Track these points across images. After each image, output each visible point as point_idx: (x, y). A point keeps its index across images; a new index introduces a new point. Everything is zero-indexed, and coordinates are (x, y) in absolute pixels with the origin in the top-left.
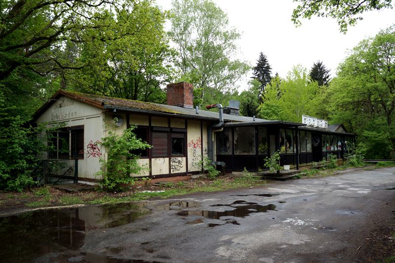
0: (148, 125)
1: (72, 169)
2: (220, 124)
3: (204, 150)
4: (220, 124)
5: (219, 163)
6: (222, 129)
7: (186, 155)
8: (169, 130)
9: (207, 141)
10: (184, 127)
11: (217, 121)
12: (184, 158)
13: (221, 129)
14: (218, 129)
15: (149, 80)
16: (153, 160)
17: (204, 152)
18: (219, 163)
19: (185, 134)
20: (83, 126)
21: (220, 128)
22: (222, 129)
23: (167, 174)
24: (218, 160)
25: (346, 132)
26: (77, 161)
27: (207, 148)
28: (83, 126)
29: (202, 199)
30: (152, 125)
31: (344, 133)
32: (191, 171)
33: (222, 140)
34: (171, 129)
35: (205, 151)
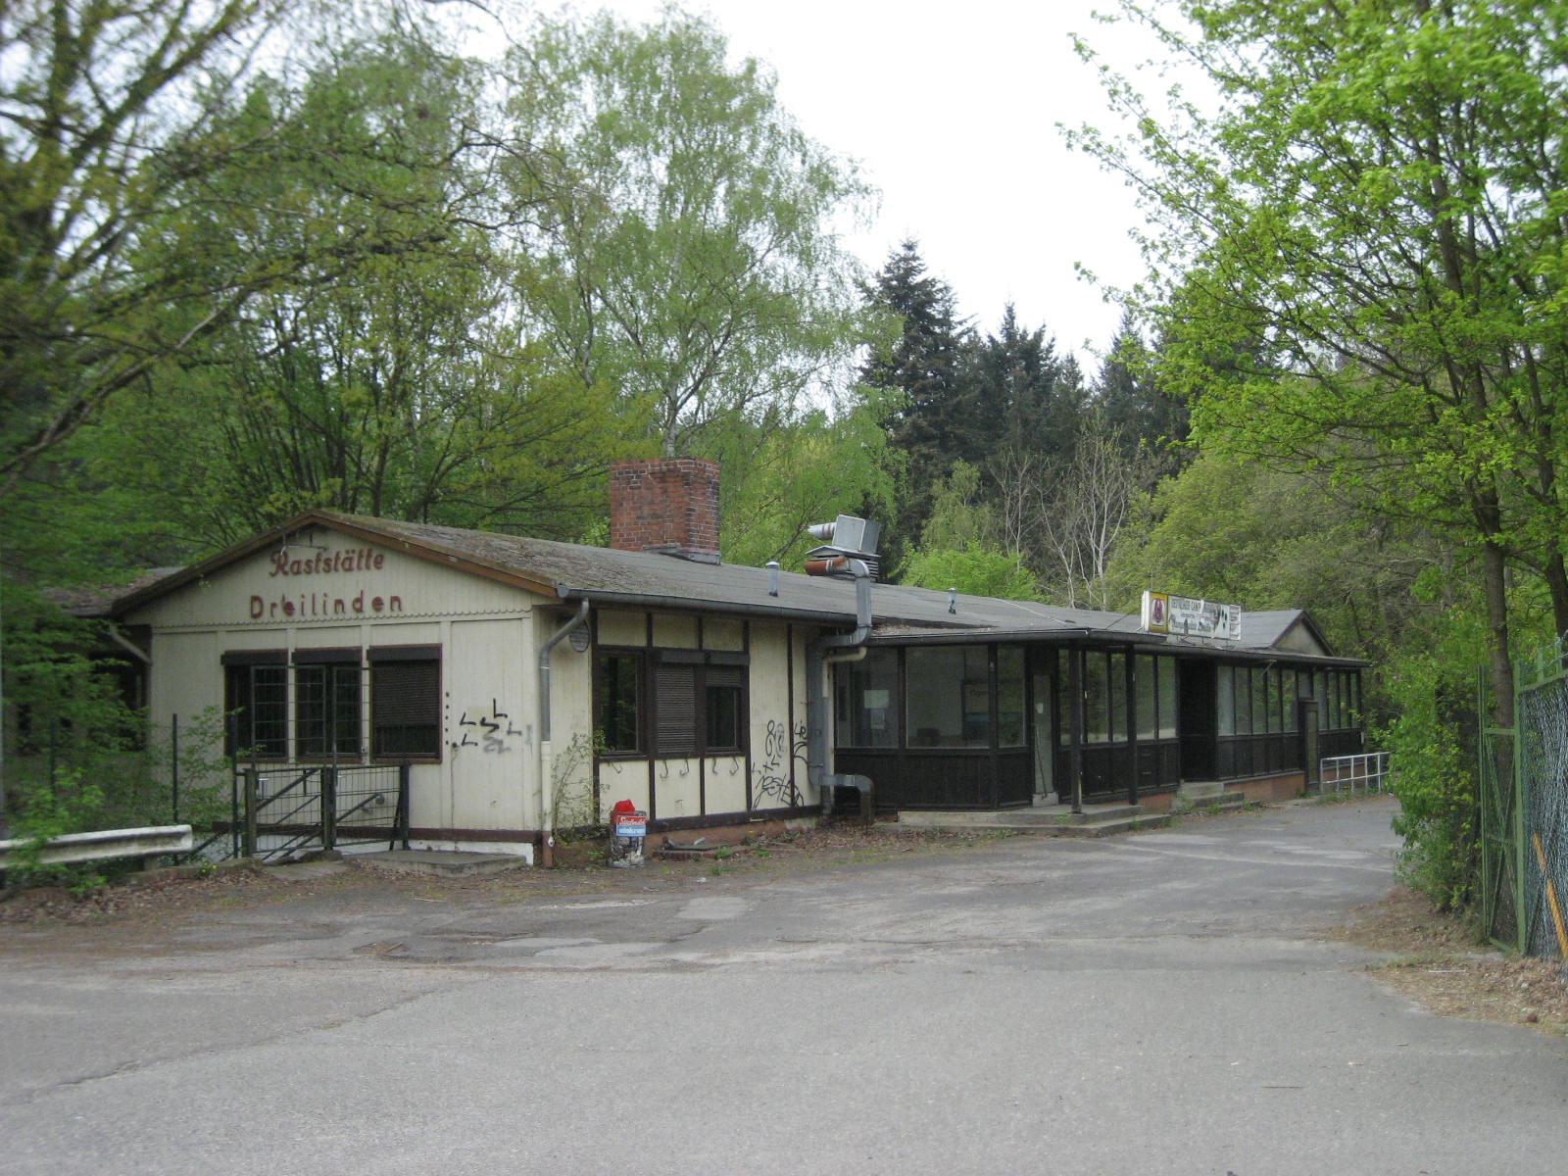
0: (640, 641)
1: (381, 801)
2: (860, 636)
3: (797, 730)
4: (860, 636)
5: (849, 781)
6: (863, 652)
7: (742, 748)
8: (699, 659)
9: (804, 700)
10: (738, 647)
11: (849, 624)
12: (741, 761)
13: (858, 652)
14: (1108, 828)
15: (473, 334)
16: (659, 765)
17: (796, 739)
18: (849, 781)
19: (743, 671)
20: (437, 649)
21: (855, 649)
22: (863, 652)
23: (695, 818)
24: (840, 769)
25: (1327, 653)
26: (407, 773)
27: (804, 724)
28: (437, 649)
29: (726, 956)
30: (657, 643)
31: (1315, 654)
32: (760, 807)
33: (851, 685)
34: (708, 654)
35: (801, 734)
